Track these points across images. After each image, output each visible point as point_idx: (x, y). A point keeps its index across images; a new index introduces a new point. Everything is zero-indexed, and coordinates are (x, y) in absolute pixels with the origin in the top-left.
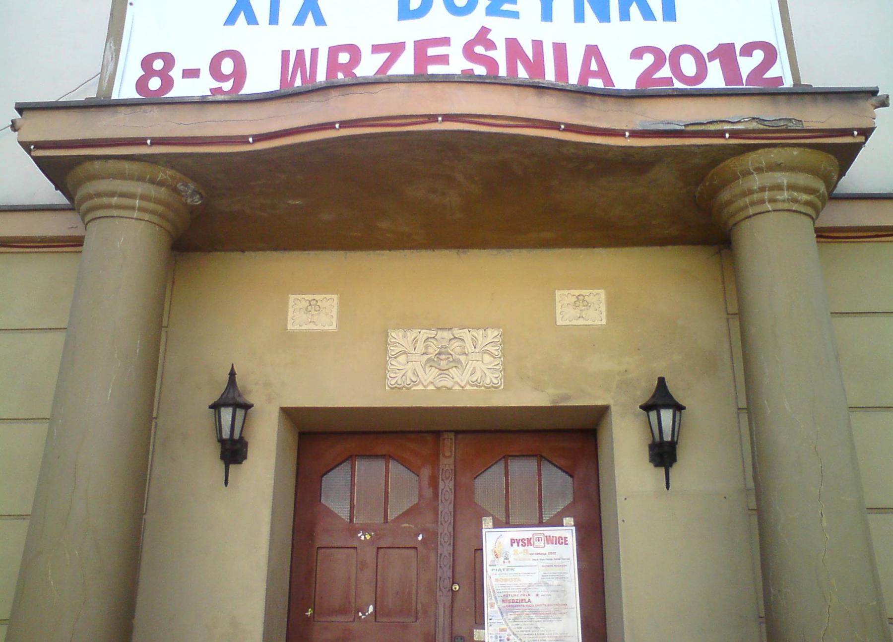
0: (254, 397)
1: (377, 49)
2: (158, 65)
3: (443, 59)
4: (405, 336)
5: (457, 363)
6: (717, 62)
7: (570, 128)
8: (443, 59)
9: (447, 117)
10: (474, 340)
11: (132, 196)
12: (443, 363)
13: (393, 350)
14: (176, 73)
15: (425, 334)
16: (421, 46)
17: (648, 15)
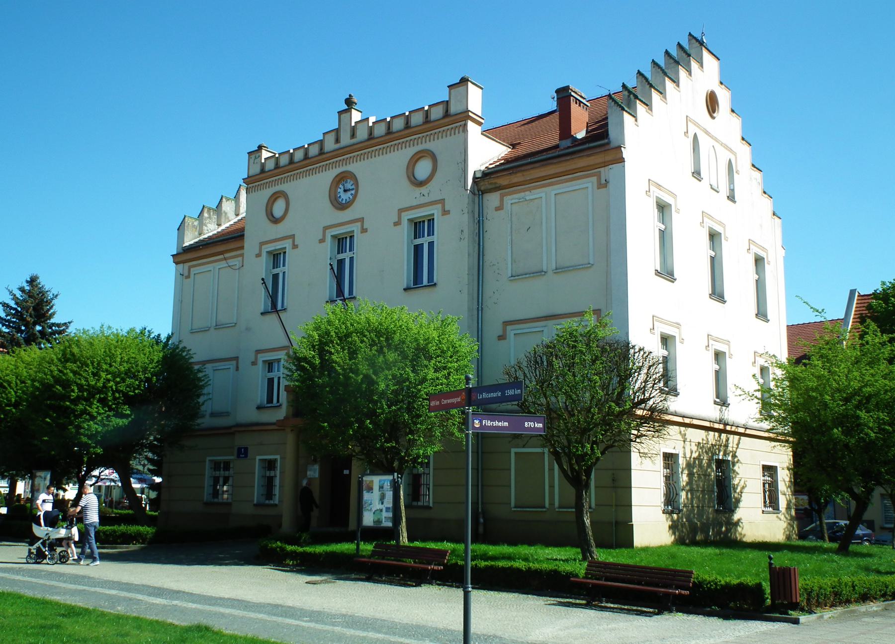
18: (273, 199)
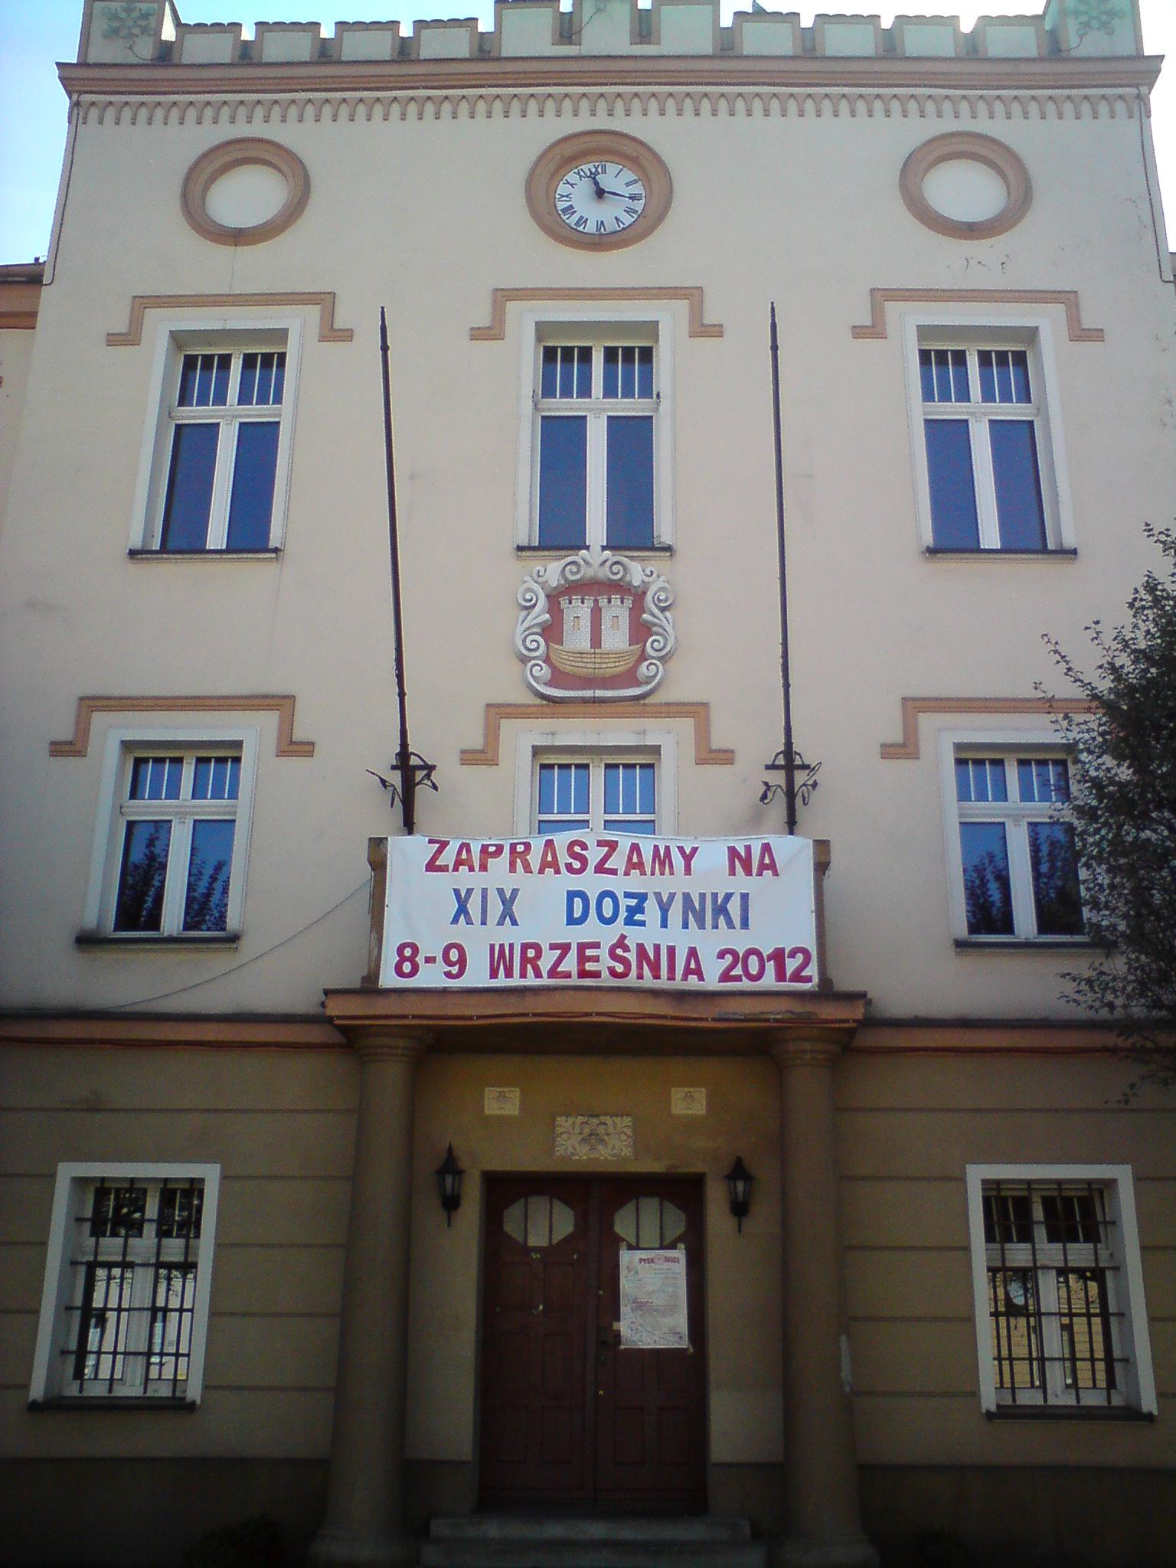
0: (464, 1164)
1: (553, 947)
2: (408, 952)
3: (596, 959)
4: (567, 1121)
5: (602, 1141)
6: (772, 962)
7: (673, 1018)
8: (596, 959)
9: (598, 1014)
10: (615, 1124)
11: (396, 1048)
12: (593, 1141)
13: (559, 1130)
14: (420, 959)
15: (580, 1119)
16: (582, 947)
17: (730, 925)
18: (219, 162)
